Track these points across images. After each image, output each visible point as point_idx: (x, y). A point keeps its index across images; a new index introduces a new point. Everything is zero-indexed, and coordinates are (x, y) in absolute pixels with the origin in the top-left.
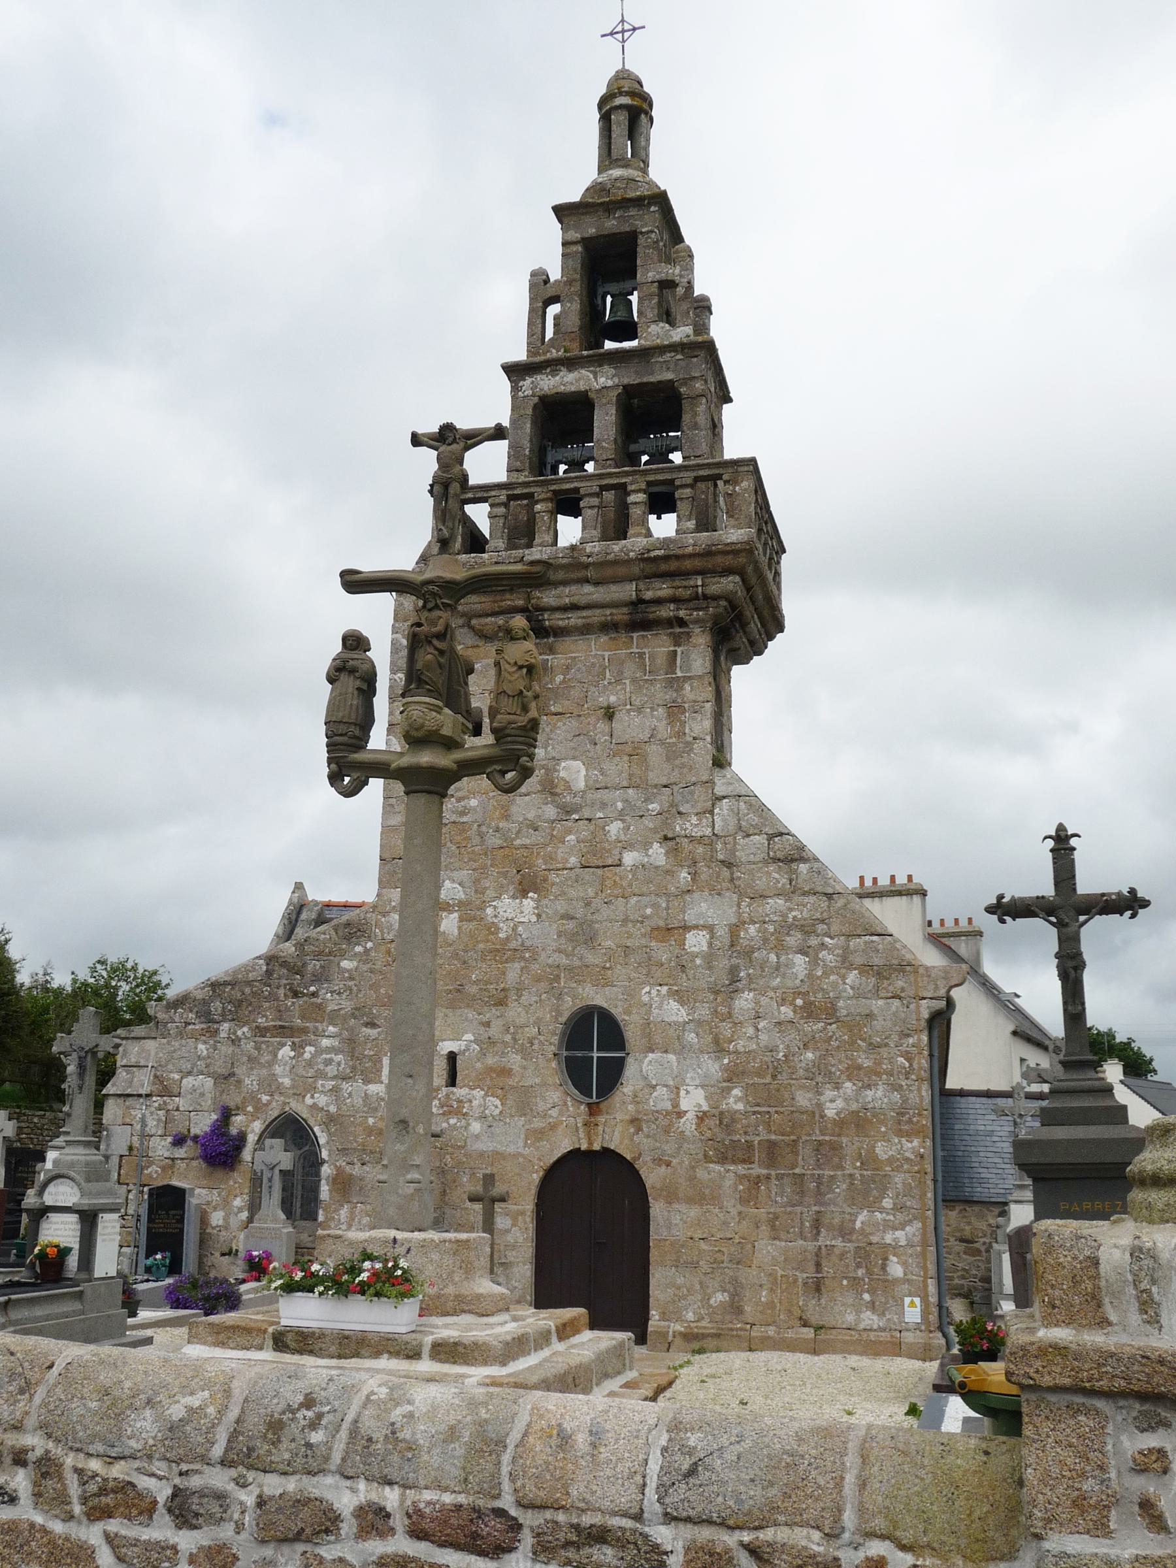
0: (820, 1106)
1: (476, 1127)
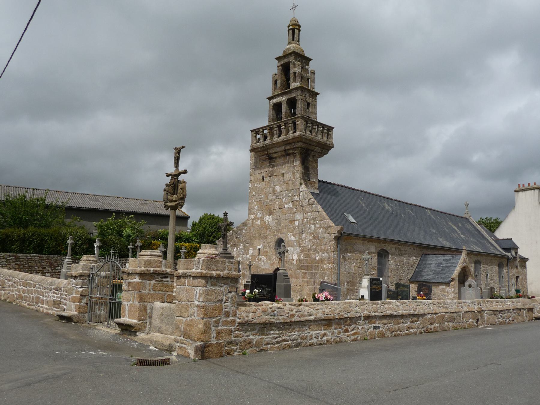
0: (315, 258)
1: (263, 263)
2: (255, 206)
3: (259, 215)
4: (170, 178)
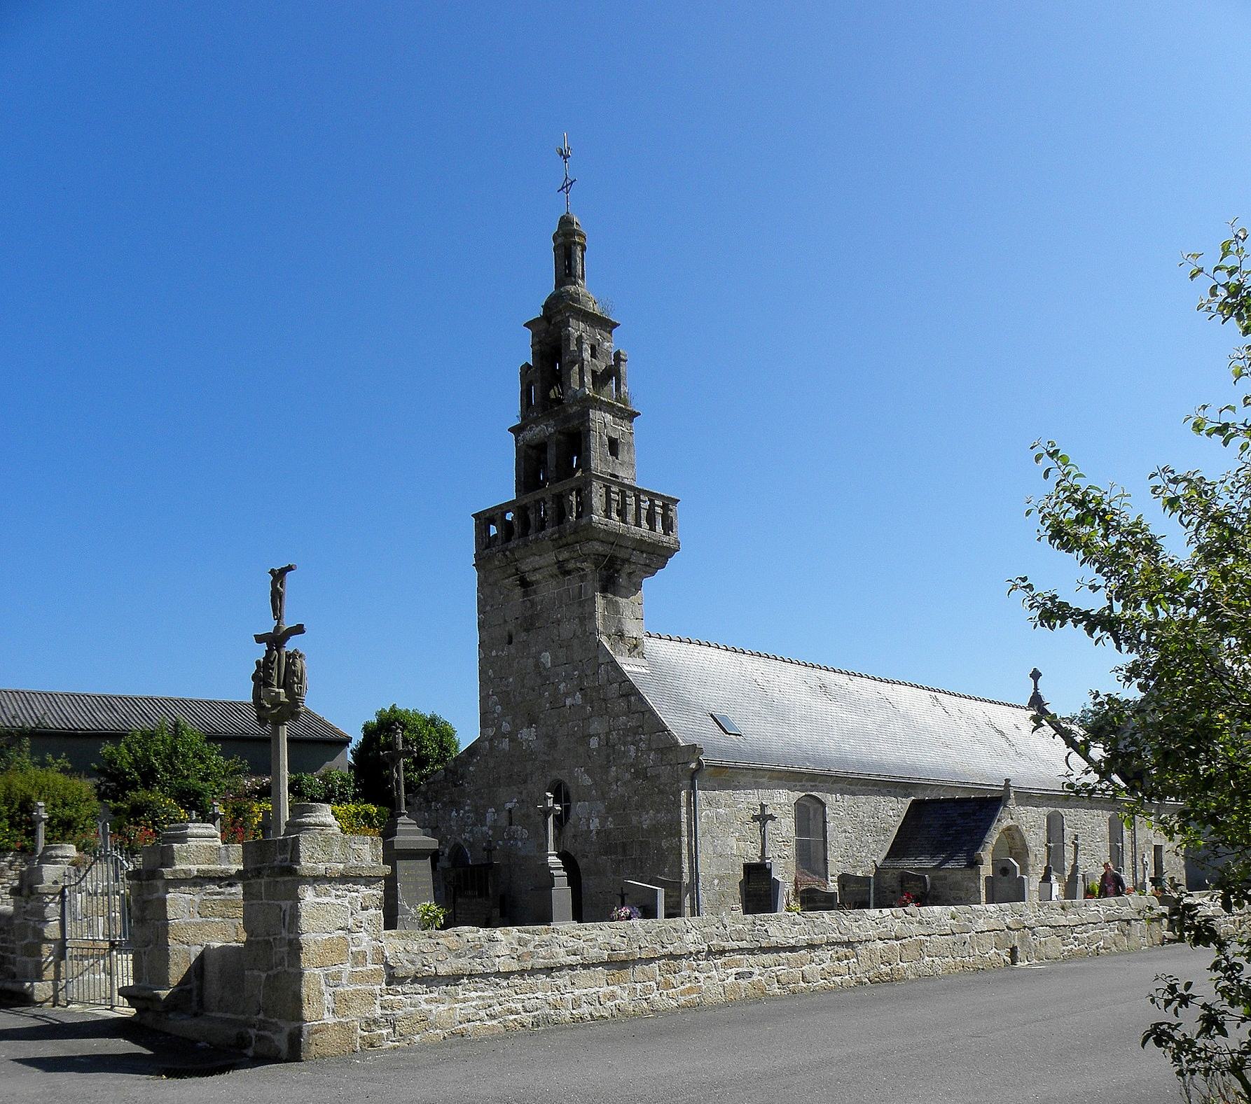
2: (496, 704)
3: (506, 727)
4: (264, 646)
